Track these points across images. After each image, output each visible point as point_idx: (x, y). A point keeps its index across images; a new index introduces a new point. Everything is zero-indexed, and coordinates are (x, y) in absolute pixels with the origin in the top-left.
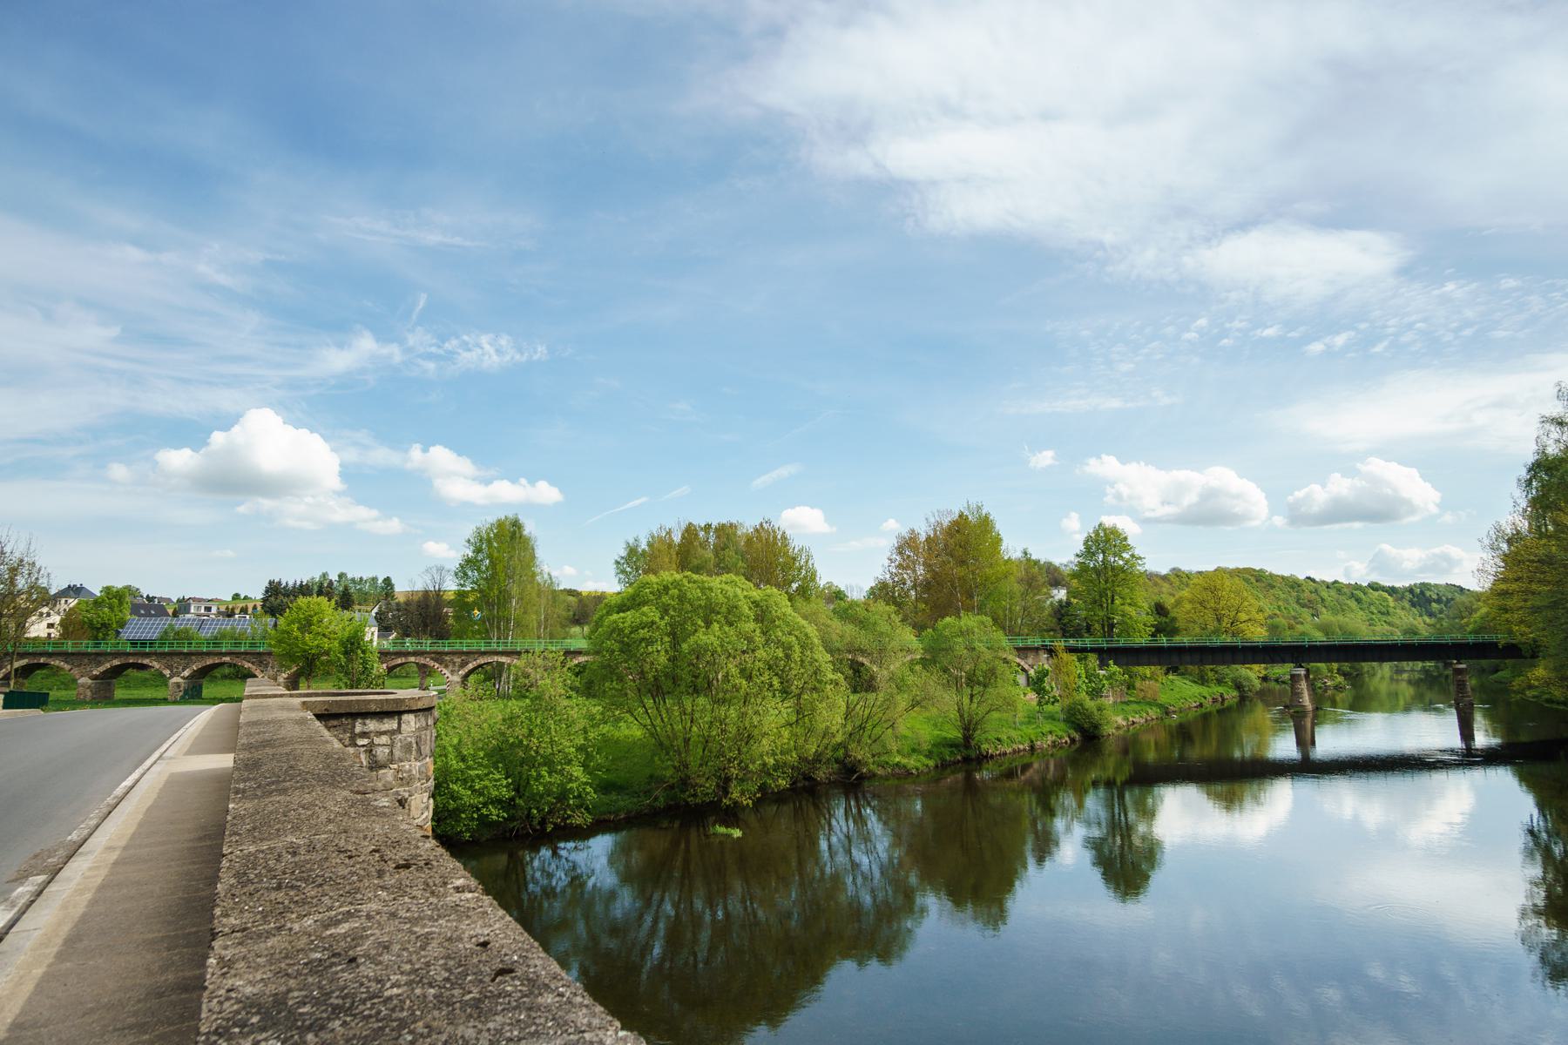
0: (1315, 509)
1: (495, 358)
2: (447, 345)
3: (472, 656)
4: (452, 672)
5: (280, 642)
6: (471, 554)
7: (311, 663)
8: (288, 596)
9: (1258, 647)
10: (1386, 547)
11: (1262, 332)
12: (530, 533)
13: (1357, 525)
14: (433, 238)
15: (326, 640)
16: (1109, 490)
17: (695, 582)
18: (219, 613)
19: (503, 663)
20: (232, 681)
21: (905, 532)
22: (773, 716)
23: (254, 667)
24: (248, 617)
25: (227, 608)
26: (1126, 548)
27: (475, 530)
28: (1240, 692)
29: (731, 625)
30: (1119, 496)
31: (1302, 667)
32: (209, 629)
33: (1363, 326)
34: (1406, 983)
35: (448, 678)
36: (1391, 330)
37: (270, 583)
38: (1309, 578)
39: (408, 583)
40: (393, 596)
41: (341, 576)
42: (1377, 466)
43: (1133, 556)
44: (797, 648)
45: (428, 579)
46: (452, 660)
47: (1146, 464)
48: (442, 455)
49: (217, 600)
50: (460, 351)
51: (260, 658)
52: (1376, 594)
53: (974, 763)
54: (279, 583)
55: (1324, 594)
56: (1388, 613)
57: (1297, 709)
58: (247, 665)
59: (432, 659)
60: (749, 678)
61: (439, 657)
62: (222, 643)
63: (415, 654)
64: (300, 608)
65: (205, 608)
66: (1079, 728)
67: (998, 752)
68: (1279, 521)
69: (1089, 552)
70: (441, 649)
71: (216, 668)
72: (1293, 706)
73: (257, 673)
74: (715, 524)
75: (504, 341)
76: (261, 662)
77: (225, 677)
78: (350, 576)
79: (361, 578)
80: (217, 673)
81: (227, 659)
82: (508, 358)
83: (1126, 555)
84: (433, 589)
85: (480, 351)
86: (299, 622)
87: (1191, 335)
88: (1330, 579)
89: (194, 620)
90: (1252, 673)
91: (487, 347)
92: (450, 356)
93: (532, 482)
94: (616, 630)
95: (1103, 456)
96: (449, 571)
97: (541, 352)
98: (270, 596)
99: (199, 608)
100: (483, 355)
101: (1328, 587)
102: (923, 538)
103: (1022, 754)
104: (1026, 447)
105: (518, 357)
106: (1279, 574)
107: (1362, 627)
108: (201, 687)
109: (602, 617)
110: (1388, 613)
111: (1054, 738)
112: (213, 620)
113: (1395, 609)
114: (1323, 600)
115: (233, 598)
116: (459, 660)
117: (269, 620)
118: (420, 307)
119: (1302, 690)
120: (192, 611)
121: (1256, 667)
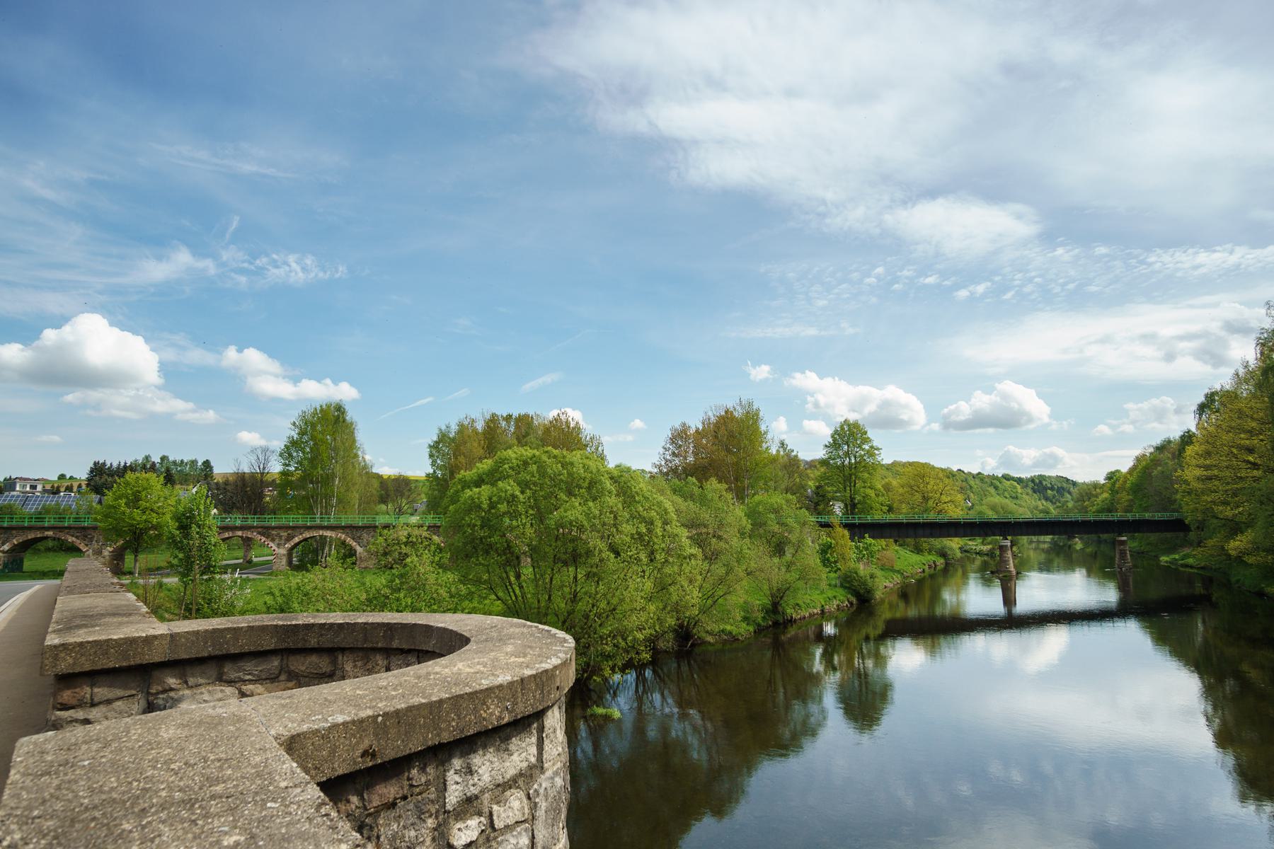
0: (962, 418)
1: (301, 274)
2: (258, 262)
3: (298, 530)
4: (279, 546)
5: (106, 516)
6: (296, 436)
7: (138, 537)
8: (112, 476)
9: (976, 523)
10: (1011, 448)
11: (924, 280)
12: (351, 418)
13: (991, 430)
14: (248, 168)
15: (154, 515)
16: (809, 399)
17: (555, 457)
18: (44, 491)
19: (326, 537)
20: (56, 554)
21: (677, 425)
22: (638, 586)
23: (79, 541)
24: (73, 494)
25: (53, 487)
26: (867, 440)
27: (301, 414)
28: (945, 559)
29: (594, 499)
30: (816, 405)
31: (1007, 539)
32: (33, 505)
33: (997, 278)
34: (1017, 777)
35: (274, 550)
36: (1017, 283)
37: (95, 464)
38: (960, 470)
39: (223, 468)
40: (212, 477)
41: (163, 458)
42: (1008, 386)
43: (872, 447)
44: (659, 523)
45: (253, 459)
46: (279, 534)
47: (840, 380)
48: (253, 357)
49: (43, 480)
50: (270, 268)
51: (85, 532)
52: (1008, 483)
53: (782, 627)
54: (104, 464)
55: (972, 483)
56: (1017, 498)
57: (1005, 574)
58: (70, 539)
59: (259, 533)
60: (617, 554)
61: (266, 531)
62: (45, 518)
63: (242, 528)
64: (127, 484)
65: (31, 486)
66: (856, 594)
67: (799, 616)
68: (936, 426)
69: (835, 445)
70: (266, 524)
71: (37, 542)
72: (1001, 571)
73: (82, 547)
74: (515, 414)
75: (309, 261)
76: (86, 537)
77: (48, 550)
78: (171, 459)
79: (182, 461)
80: (40, 546)
81: (50, 533)
82: (312, 275)
83: (866, 447)
84: (258, 471)
85: (287, 268)
86: (127, 498)
87: (872, 280)
88: (975, 472)
89: (18, 496)
90: (954, 544)
91: (294, 265)
92: (260, 271)
93: (335, 382)
94: (474, 506)
95: (807, 371)
96: (273, 452)
97: (342, 272)
98: (95, 476)
99: (24, 486)
100: (290, 271)
101: (973, 477)
102: (692, 431)
103: (816, 616)
104: (749, 362)
105: (321, 275)
106: (939, 466)
107: (990, 507)
108: (22, 561)
109: (457, 492)
110: (1017, 498)
111: (838, 602)
112: (38, 497)
113: (1022, 494)
114: (971, 487)
115: (59, 478)
116: (286, 534)
117: (95, 497)
118: (233, 227)
119: (1009, 558)
120: (18, 489)
121: (956, 539)
